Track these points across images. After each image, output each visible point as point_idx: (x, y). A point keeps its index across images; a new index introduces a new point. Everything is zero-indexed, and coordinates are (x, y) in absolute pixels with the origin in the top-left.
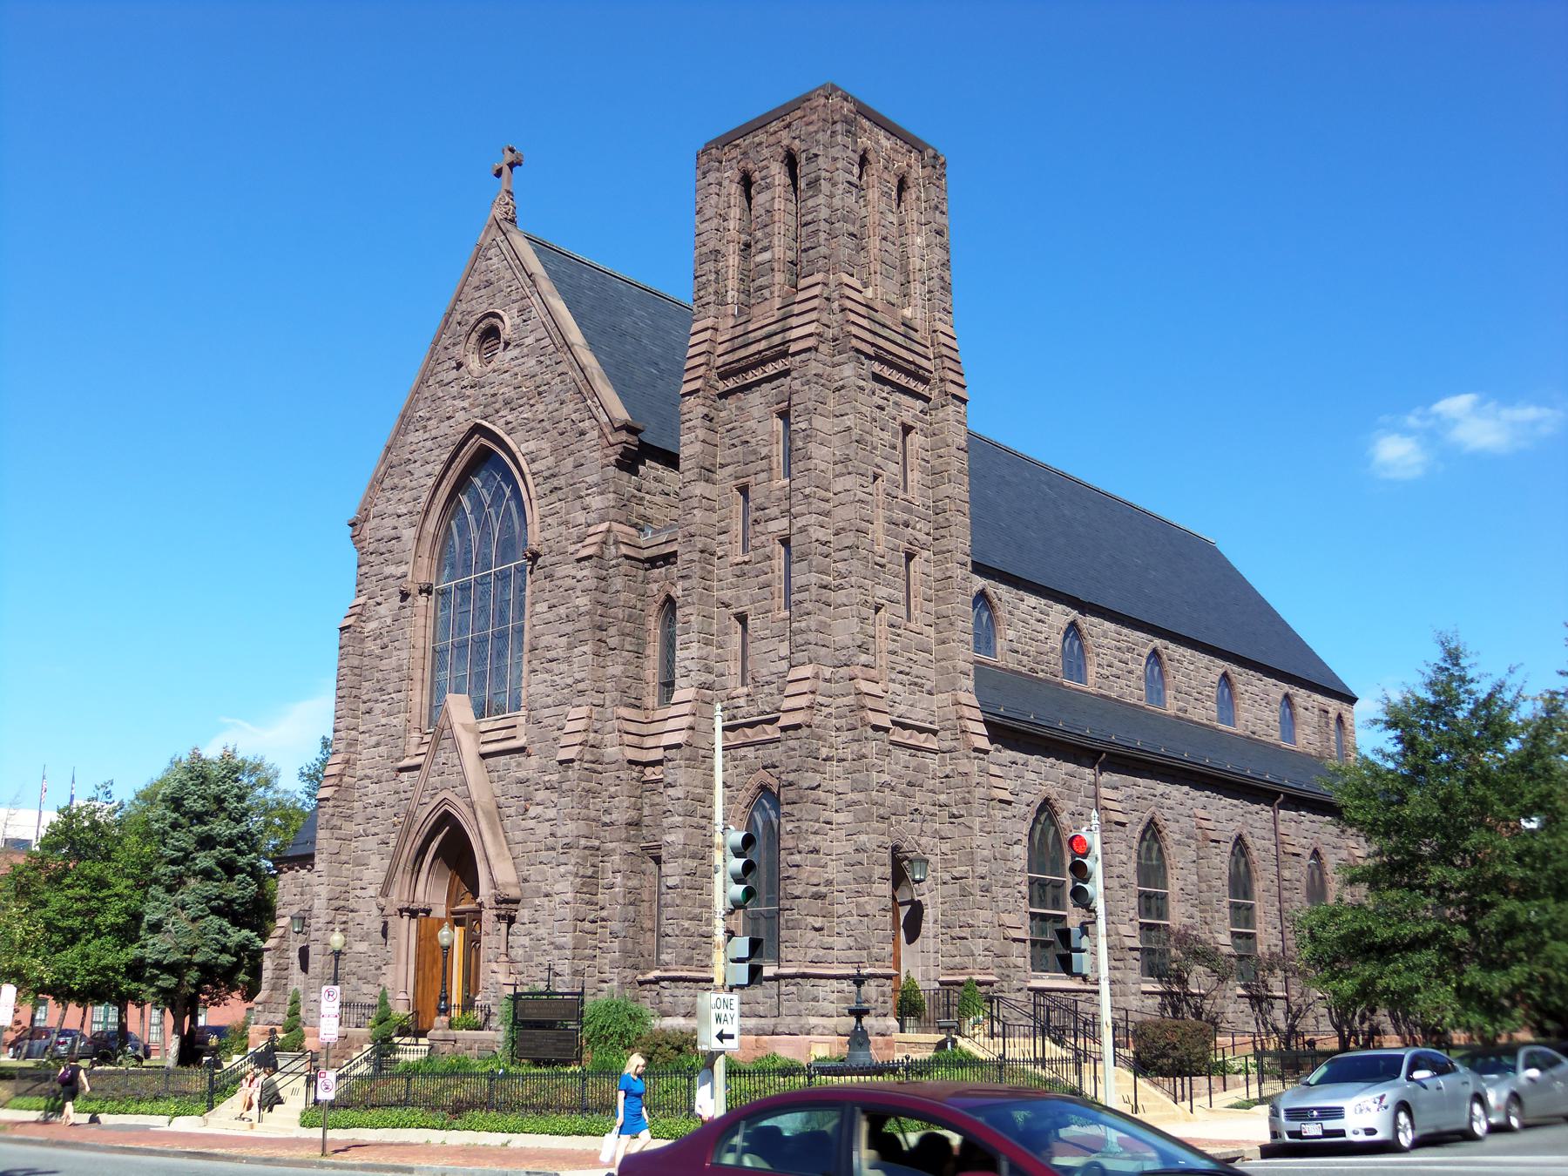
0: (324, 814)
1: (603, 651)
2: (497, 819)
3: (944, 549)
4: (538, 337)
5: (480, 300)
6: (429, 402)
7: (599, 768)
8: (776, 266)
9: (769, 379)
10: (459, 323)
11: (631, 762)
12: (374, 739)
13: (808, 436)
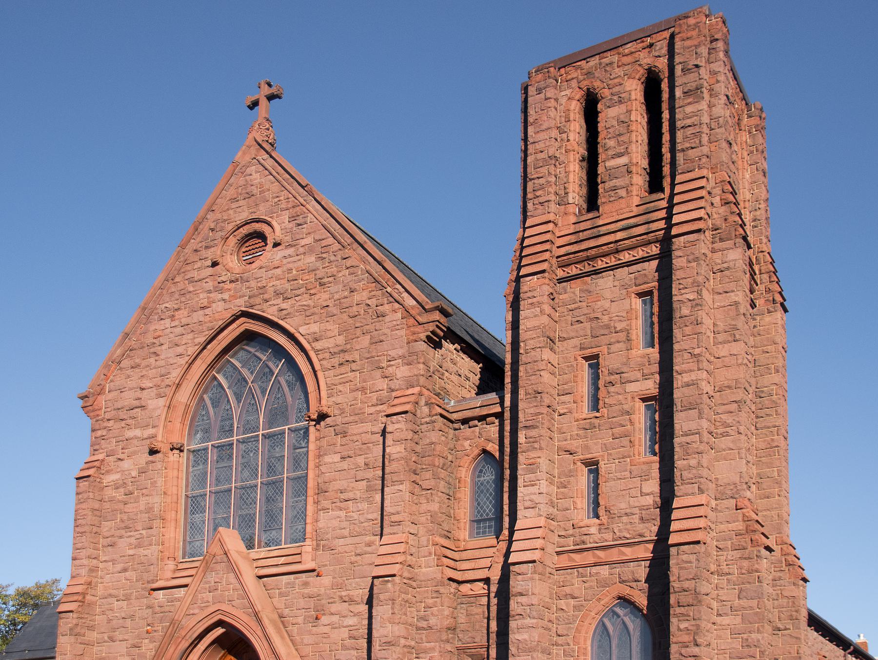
0: (67, 623)
1: (417, 490)
2: (282, 626)
3: (770, 425)
4: (317, 238)
5: (238, 210)
6: (176, 296)
7: (414, 584)
8: (634, 169)
9: (629, 264)
10: (212, 230)
11: (450, 579)
12: (119, 567)
13: (697, 305)
